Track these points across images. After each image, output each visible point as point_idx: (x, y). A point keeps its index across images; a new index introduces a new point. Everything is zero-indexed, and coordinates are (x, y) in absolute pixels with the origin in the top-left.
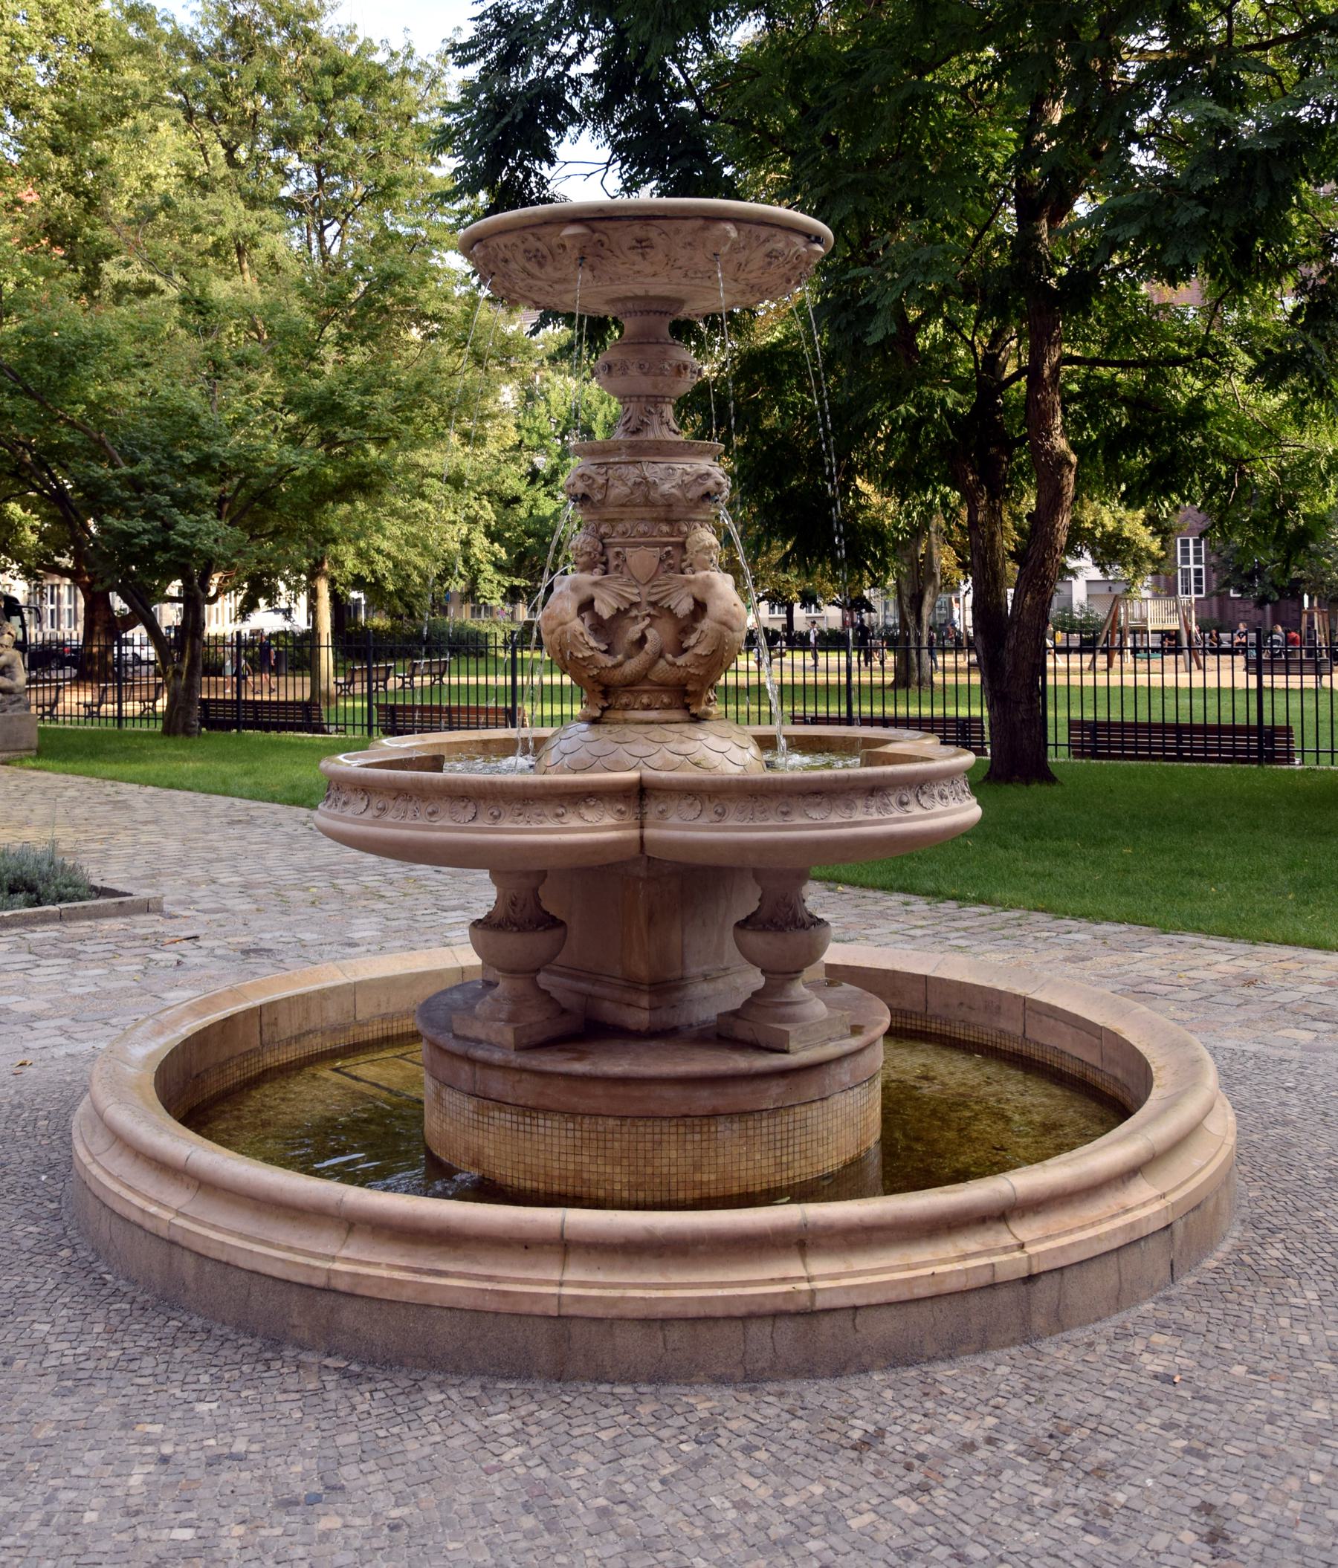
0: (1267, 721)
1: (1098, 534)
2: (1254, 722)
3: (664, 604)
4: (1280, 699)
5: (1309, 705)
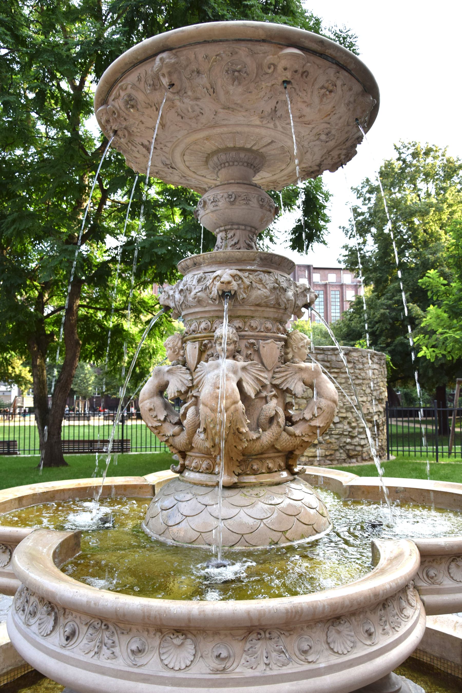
0: (125, 438)
1: (13, 375)
2: (120, 438)
3: (284, 387)
4: (76, 429)
5: (86, 430)
